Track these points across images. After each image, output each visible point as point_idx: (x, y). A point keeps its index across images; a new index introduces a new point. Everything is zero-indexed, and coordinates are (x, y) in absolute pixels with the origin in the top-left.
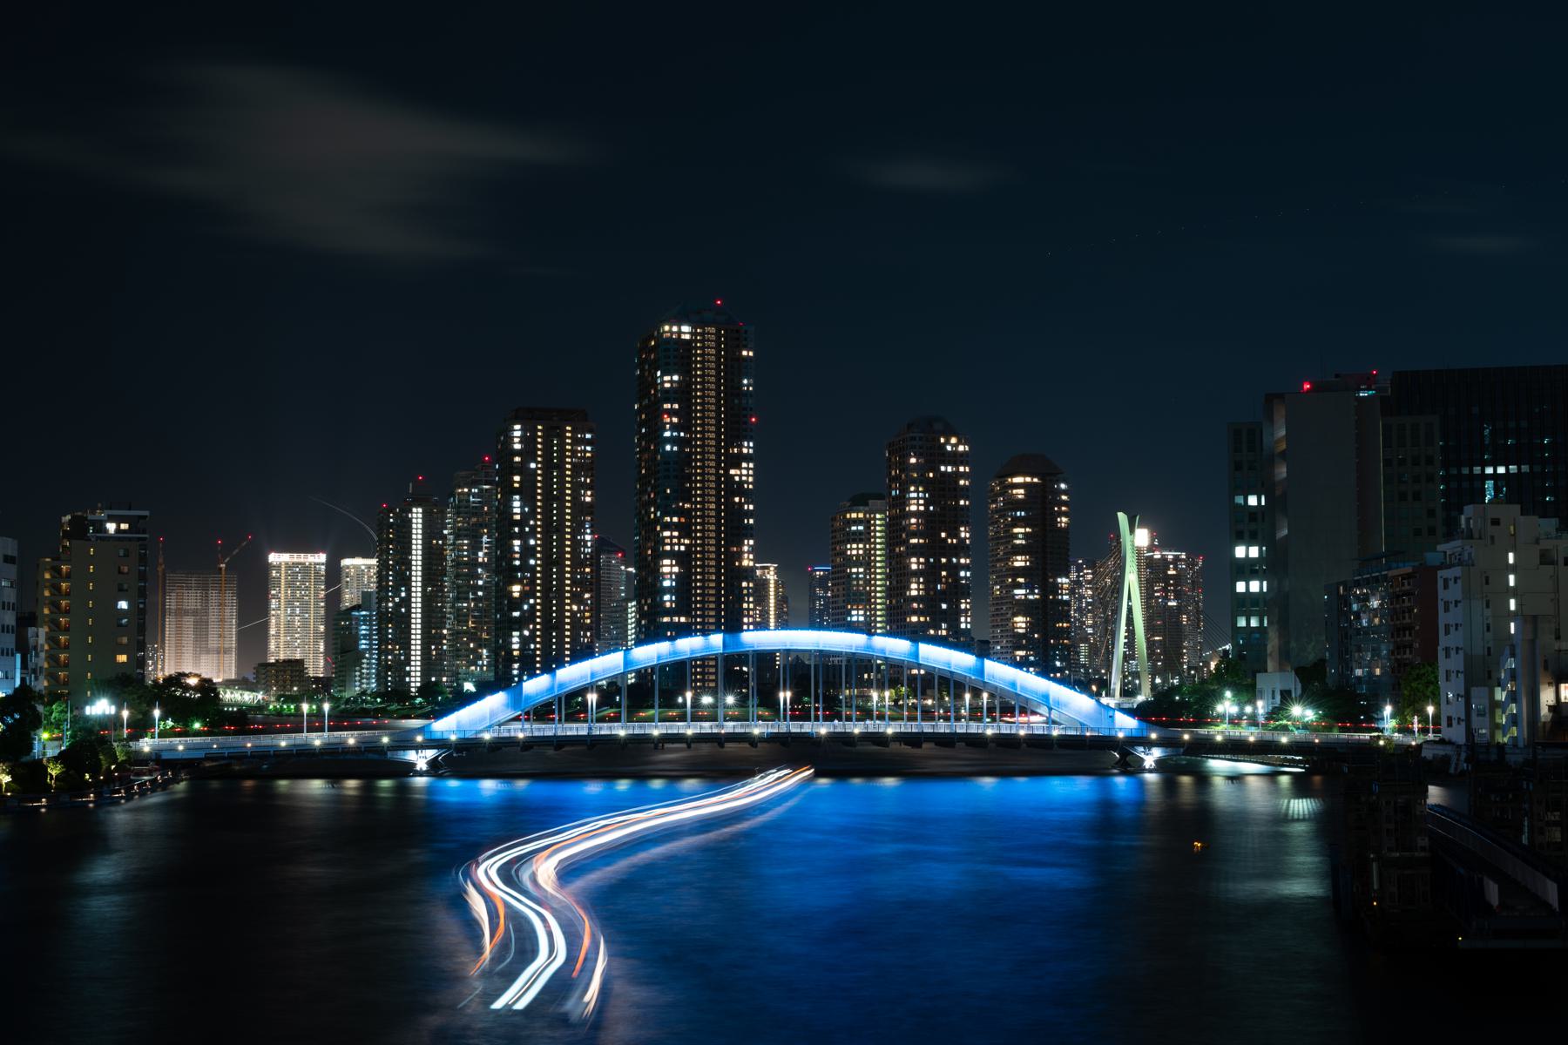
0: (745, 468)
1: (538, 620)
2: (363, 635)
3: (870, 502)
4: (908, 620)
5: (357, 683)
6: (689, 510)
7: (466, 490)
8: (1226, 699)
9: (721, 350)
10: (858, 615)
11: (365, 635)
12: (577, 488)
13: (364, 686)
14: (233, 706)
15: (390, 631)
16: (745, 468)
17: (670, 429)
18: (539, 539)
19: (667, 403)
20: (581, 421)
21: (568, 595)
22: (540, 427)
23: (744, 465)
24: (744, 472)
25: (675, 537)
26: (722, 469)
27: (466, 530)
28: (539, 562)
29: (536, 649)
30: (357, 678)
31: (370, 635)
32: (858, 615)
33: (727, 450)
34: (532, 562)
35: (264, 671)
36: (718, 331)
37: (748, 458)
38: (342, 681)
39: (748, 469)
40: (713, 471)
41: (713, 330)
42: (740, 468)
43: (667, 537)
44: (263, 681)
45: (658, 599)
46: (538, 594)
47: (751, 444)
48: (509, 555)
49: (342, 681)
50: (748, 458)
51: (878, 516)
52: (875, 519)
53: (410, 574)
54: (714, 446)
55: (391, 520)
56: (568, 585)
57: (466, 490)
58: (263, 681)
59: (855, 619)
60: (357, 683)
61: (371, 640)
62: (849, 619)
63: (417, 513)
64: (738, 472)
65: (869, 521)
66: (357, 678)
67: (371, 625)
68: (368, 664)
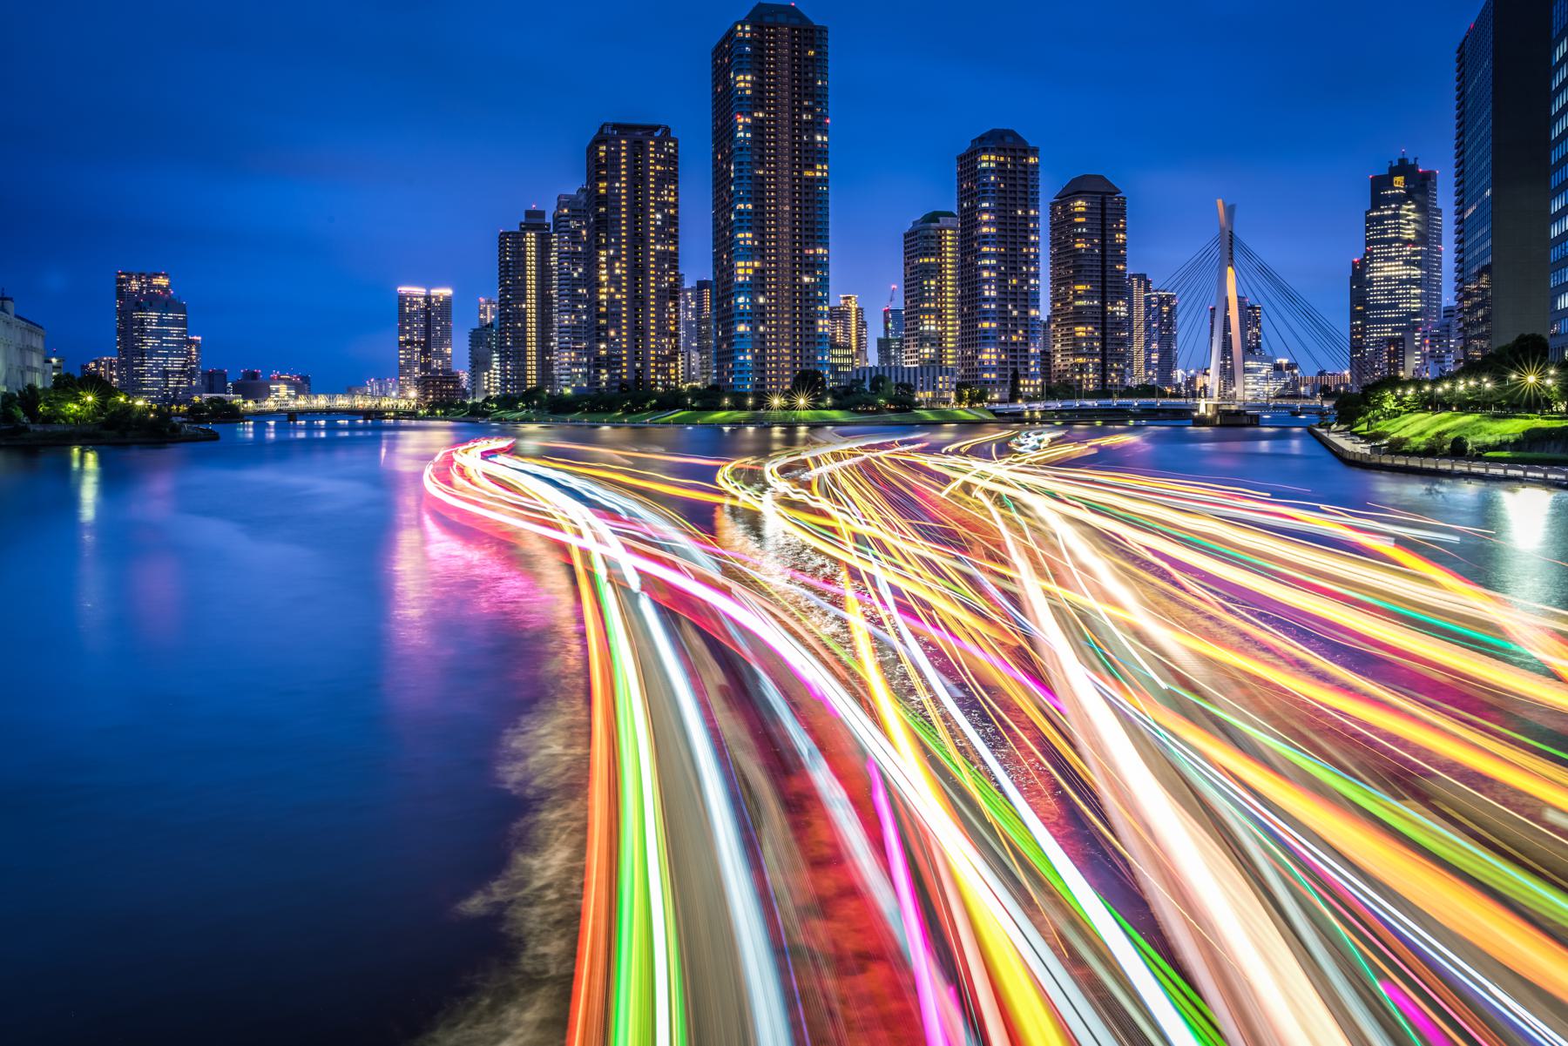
0: (819, 170)
1: (624, 334)
3: (941, 219)
4: (980, 326)
6: (762, 177)
10: (930, 325)
16: (819, 170)
17: (743, 130)
18: (624, 262)
19: (741, 260)
21: (652, 278)
23: (819, 167)
25: (749, 239)
28: (624, 297)
29: (620, 188)
32: (930, 325)
42: (815, 170)
43: (741, 239)
45: (733, 302)
46: (623, 179)
51: (948, 232)
52: (946, 235)
56: (652, 152)
59: (927, 328)
62: (921, 328)
65: (940, 310)
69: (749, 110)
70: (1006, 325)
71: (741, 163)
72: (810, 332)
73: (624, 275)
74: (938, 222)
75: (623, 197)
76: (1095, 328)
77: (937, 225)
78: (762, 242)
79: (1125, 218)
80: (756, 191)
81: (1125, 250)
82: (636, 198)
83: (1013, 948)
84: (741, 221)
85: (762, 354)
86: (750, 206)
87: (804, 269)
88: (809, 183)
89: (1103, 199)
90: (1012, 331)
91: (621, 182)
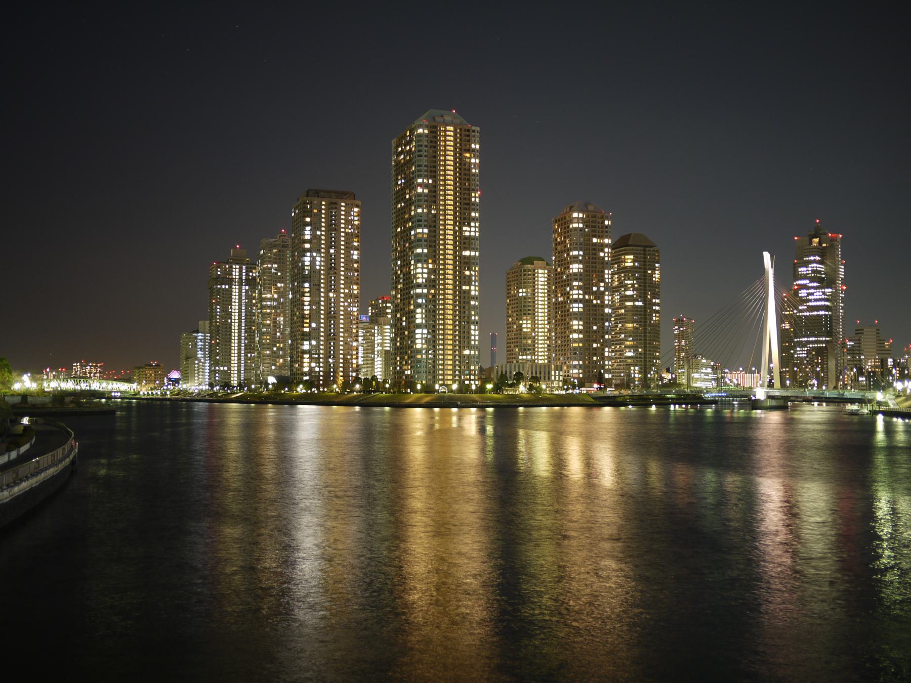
2: (200, 339)
3: (535, 262)
5: (196, 375)
7: (269, 266)
8: (879, 432)
9: (457, 162)
11: (201, 349)
12: (349, 247)
13: (201, 380)
14: (117, 392)
15: (218, 310)
20: (349, 196)
22: (323, 203)
24: (473, 229)
26: (457, 226)
27: (268, 345)
30: (196, 369)
31: (205, 348)
33: (460, 352)
34: (318, 233)
35: (137, 371)
36: (455, 130)
37: (475, 220)
38: (186, 376)
39: (475, 227)
40: (451, 227)
41: (451, 128)
44: (137, 375)
46: (323, 229)
47: (477, 269)
48: (301, 290)
49: (186, 376)
50: (475, 220)
53: (231, 321)
54: (451, 335)
55: (219, 273)
57: (269, 266)
58: (137, 375)
60: (196, 375)
61: (205, 351)
63: (236, 268)
64: (468, 229)
66: (196, 369)
67: (205, 351)
68: (202, 375)
69: (426, 258)
70: (590, 319)
71: (419, 166)
72: (467, 172)
73: (323, 270)
74: (533, 264)
75: (321, 378)
76: (640, 325)
77: (533, 266)
78: (434, 336)
79: (659, 253)
80: (431, 171)
81: (659, 288)
82: (331, 221)
83: (573, 403)
84: (420, 151)
85: (434, 299)
86: (426, 251)
87: (463, 246)
88: (466, 260)
89: (645, 251)
90: (593, 353)
91: (321, 231)
